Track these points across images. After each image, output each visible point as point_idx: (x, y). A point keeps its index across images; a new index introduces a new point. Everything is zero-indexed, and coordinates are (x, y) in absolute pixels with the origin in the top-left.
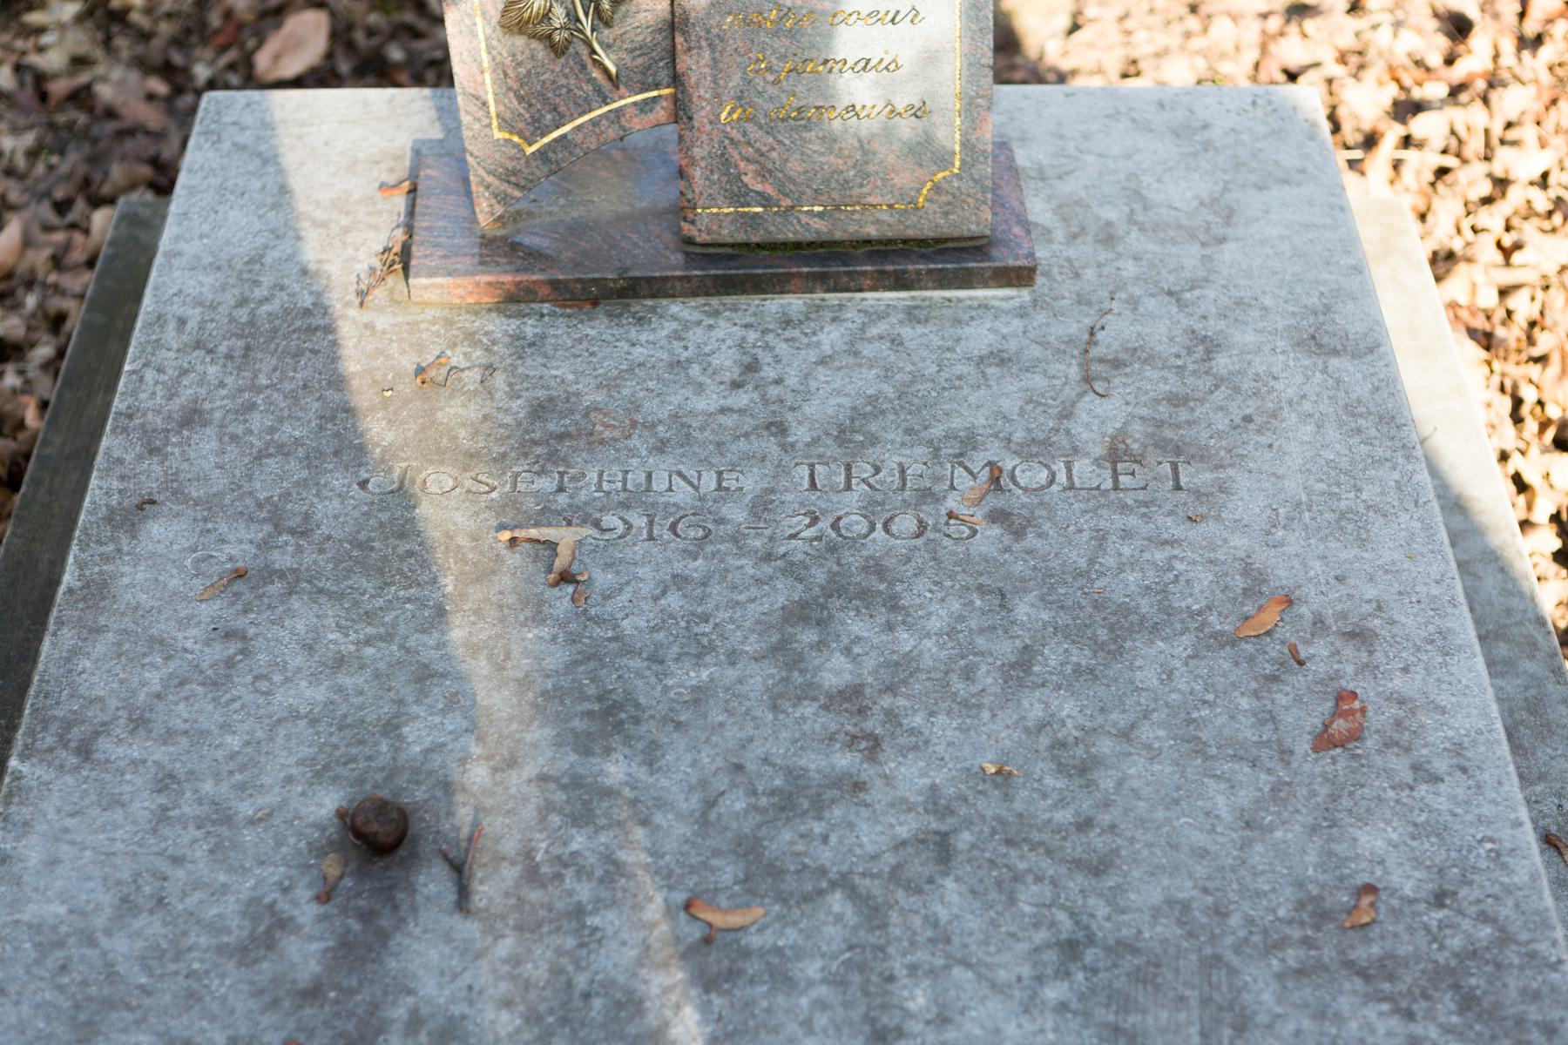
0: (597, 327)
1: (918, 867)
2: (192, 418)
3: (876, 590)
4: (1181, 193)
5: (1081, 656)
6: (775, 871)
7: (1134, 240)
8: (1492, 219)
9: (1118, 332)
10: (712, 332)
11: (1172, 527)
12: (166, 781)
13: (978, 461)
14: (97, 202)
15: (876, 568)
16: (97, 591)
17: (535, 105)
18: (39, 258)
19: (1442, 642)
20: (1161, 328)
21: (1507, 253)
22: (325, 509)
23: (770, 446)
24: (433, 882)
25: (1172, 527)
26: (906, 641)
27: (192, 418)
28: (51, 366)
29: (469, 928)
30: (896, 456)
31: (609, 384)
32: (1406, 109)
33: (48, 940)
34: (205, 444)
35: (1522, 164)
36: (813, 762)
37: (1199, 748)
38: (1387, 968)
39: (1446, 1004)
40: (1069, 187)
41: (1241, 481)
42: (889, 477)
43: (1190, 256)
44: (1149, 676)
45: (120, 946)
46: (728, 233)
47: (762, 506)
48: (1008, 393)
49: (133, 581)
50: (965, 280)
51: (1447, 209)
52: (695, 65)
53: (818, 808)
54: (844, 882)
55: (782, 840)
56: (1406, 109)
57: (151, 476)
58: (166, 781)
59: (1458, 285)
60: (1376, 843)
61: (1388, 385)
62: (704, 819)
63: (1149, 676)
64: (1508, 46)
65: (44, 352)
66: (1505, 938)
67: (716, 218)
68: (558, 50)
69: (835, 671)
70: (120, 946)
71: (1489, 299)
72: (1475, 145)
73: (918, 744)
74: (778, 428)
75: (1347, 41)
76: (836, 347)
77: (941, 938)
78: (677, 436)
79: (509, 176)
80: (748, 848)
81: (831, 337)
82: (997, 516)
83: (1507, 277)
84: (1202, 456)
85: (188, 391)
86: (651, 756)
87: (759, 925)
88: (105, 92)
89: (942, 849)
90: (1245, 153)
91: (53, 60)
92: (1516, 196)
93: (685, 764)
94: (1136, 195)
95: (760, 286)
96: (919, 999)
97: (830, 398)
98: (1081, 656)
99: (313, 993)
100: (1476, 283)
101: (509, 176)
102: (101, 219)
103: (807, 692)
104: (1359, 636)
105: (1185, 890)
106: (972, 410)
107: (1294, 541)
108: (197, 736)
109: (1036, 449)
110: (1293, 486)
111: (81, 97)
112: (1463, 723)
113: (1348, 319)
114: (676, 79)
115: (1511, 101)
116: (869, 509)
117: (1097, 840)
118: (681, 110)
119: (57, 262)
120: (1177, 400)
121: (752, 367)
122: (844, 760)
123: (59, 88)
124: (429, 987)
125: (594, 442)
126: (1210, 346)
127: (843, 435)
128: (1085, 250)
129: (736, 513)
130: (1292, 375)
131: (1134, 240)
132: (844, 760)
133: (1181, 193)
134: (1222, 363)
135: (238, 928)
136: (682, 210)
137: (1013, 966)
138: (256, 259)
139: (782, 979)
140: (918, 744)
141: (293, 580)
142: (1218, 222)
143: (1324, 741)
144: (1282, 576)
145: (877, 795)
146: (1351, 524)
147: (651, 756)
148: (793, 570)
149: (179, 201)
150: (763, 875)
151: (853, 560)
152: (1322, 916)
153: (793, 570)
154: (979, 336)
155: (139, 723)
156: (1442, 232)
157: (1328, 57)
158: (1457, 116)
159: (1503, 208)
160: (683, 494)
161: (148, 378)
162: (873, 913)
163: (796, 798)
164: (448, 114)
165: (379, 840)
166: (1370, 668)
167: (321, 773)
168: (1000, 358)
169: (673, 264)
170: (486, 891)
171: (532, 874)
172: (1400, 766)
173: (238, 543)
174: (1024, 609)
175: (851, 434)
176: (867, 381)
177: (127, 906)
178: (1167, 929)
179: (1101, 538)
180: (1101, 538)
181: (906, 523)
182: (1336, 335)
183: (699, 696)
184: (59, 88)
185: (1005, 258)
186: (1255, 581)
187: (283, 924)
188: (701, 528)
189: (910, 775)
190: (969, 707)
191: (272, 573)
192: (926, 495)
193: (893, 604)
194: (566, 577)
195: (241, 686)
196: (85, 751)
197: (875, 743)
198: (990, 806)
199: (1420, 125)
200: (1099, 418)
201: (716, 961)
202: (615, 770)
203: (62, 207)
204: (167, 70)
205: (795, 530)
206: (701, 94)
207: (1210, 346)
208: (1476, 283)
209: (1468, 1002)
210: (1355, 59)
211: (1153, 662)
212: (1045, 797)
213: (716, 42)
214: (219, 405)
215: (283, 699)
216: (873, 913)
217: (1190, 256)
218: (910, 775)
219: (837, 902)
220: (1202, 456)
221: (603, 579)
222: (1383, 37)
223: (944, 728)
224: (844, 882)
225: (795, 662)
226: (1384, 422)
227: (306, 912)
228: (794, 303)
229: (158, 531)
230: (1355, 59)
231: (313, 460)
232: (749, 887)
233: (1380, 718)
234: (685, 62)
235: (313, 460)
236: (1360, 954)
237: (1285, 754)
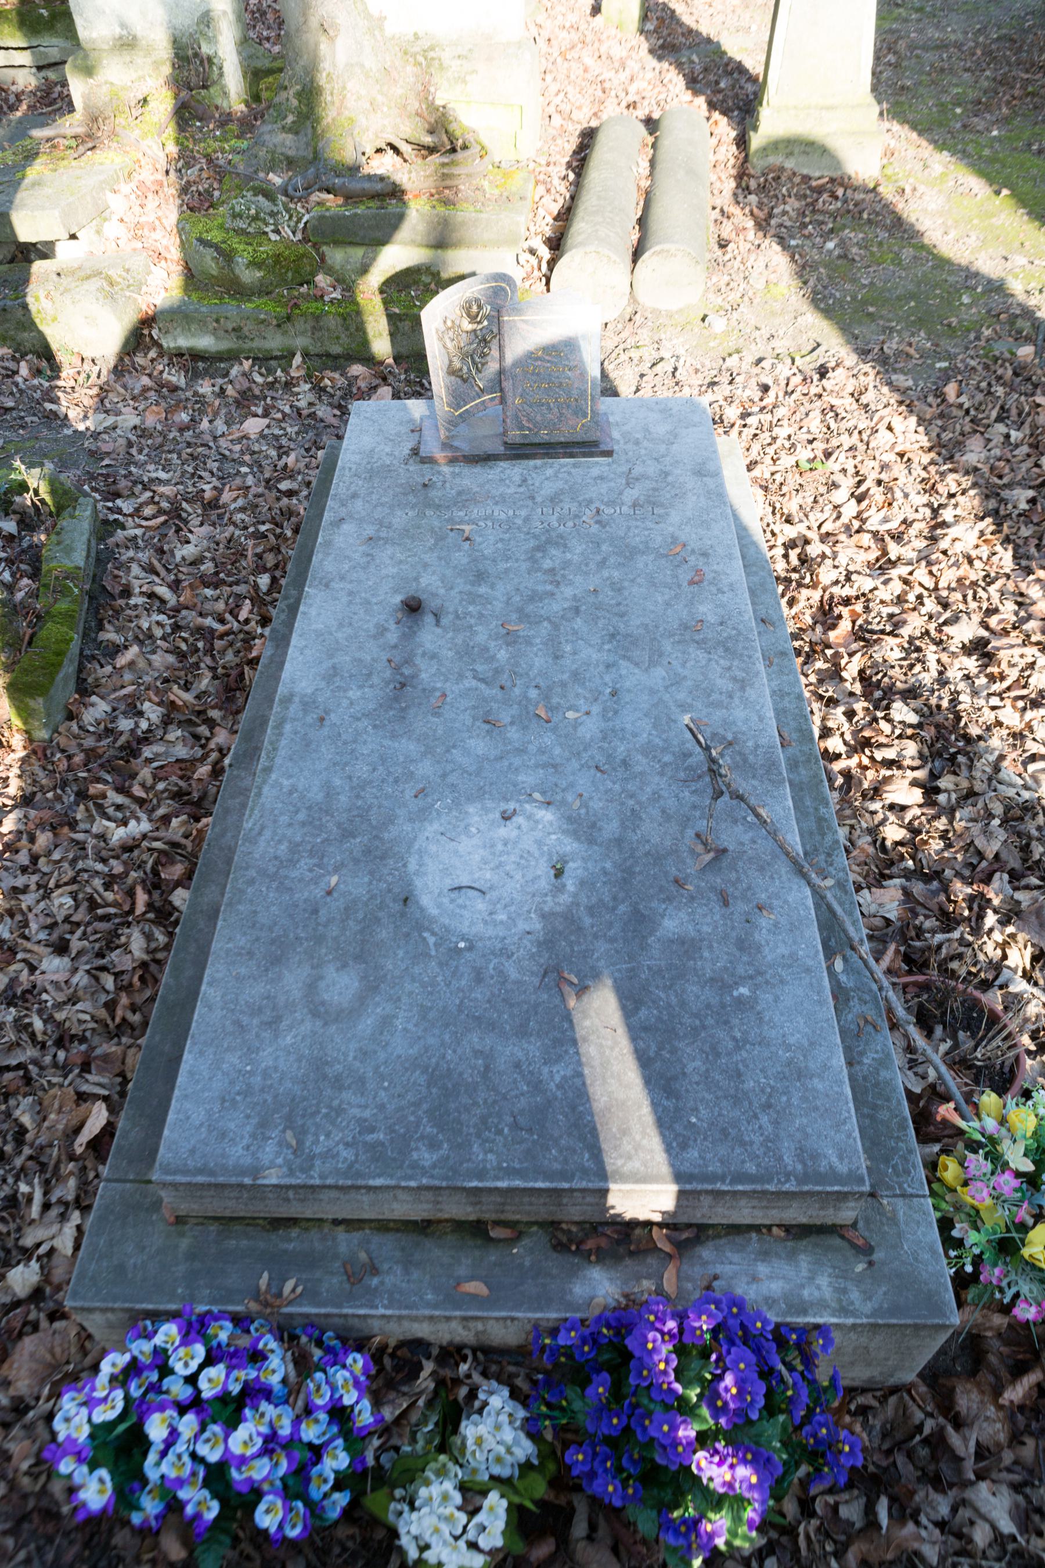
0: (477, 469)
1: (569, 615)
2: (354, 496)
3: (561, 542)
4: (661, 429)
5: (621, 560)
6: (528, 616)
7: (645, 443)
8: (771, 450)
9: (638, 470)
10: (513, 471)
11: (650, 525)
12: (350, 593)
13: (593, 507)
14: (319, 449)
15: (561, 536)
16: (328, 544)
17: (457, 399)
18: (301, 465)
19: (730, 557)
20: (652, 469)
21: (774, 461)
22: (395, 521)
23: (530, 503)
24: (429, 619)
25: (650, 525)
26: (569, 556)
27: (354, 496)
28: (307, 497)
29: (439, 631)
30: (568, 506)
31: (481, 486)
32: (745, 415)
33: (319, 634)
34: (359, 504)
35: (782, 432)
36: (540, 588)
37: (654, 585)
38: (704, 641)
39: (720, 651)
40: (625, 428)
41: (673, 513)
42: (566, 511)
43: (663, 448)
44: (641, 565)
45: (339, 635)
46: (518, 440)
47: (527, 519)
48: (603, 488)
49: (339, 540)
50: (591, 455)
51: (756, 447)
52: (507, 385)
53: (541, 600)
54: (548, 619)
55: (530, 608)
56: (745, 415)
57: (343, 512)
58: (350, 593)
59: (757, 472)
60: (705, 610)
61: (721, 485)
62: (507, 603)
63: (641, 565)
64: (781, 394)
65: (305, 493)
66: (739, 633)
67: (515, 435)
68: (465, 381)
69: (547, 564)
70: (339, 635)
71: (767, 475)
72: (766, 426)
73: (571, 583)
74: (533, 498)
75: (727, 393)
76: (549, 475)
77: (575, 632)
78: (502, 500)
79: (450, 422)
80: (520, 610)
81: (549, 472)
82: (597, 522)
83: (774, 469)
84: (662, 505)
85: (353, 488)
86: (492, 586)
87: (522, 629)
88: (320, 414)
89: (577, 611)
90: (678, 416)
91: (302, 404)
92: (779, 442)
93: (501, 590)
94: (647, 430)
95: (527, 457)
96: (568, 648)
97: (549, 489)
98: (621, 560)
99: (395, 647)
100: (763, 471)
101: (450, 422)
102: (320, 454)
103: (539, 570)
104: (705, 555)
105: (647, 621)
106: (592, 492)
107: (688, 529)
108: (359, 582)
109: (611, 503)
110: (689, 514)
111: (312, 416)
112: (733, 578)
113: (711, 466)
114: (502, 390)
115: (780, 412)
116: (559, 520)
117: (622, 608)
118: (503, 401)
119: (307, 466)
120: (655, 490)
121: (525, 481)
122: (549, 587)
123: (305, 412)
124: (428, 645)
125: (476, 502)
126: (667, 474)
127: (552, 500)
128: (630, 447)
129: (519, 522)
130: (691, 482)
131: (645, 443)
132: (549, 587)
133: (661, 429)
134: (670, 479)
135: (373, 631)
136: (505, 433)
137: (596, 640)
138: (372, 451)
139: (528, 642)
140: (571, 583)
141: (386, 541)
142: (673, 437)
143: (691, 583)
144: (683, 538)
145: (558, 596)
146: (706, 524)
147: (492, 586)
148: (535, 537)
149: (345, 442)
150: (524, 616)
151: (553, 534)
152: (686, 628)
153: (535, 537)
154: (595, 472)
155: (342, 578)
156: (754, 455)
157: (721, 398)
158: (762, 417)
159: (774, 447)
160: (503, 516)
161: (339, 485)
162: (556, 627)
163: (534, 597)
164: (432, 408)
165: (413, 607)
166: (707, 564)
167: (396, 591)
168: (601, 478)
169: (501, 449)
170: (444, 621)
171: (457, 617)
172: (714, 589)
173: (370, 530)
174: (604, 547)
175: (554, 500)
176: (560, 484)
177: (341, 625)
178: (641, 631)
179: (629, 528)
180: (629, 528)
181: (570, 524)
182: (707, 471)
183: (507, 571)
184: (305, 412)
185: (603, 447)
186: (675, 540)
187: (386, 629)
188: (509, 525)
189: (568, 591)
190: (586, 573)
191: (379, 538)
192: (577, 516)
193: (565, 546)
194: (467, 539)
195: (372, 569)
196: (327, 586)
197: (558, 583)
198: (591, 599)
199: (749, 420)
200: (630, 495)
201: (510, 639)
202: (483, 590)
203: (307, 450)
204: (339, 407)
205: (537, 526)
206: (509, 394)
207: (667, 474)
208: (763, 471)
209: (727, 650)
210: (730, 400)
211: (640, 562)
212: (607, 596)
213: (514, 377)
214: (362, 492)
215: (384, 572)
216: (556, 627)
217: (663, 448)
218: (568, 591)
219: (545, 624)
220: (662, 505)
221: (479, 539)
222: (739, 392)
223: (578, 579)
224: (548, 619)
225: (536, 561)
226: (719, 496)
227: (393, 626)
228: (538, 462)
229: (346, 527)
230: (730, 400)
231: (392, 507)
232: (520, 620)
233: (709, 576)
234: (504, 384)
235: (392, 507)
236: (697, 638)
237: (679, 586)
